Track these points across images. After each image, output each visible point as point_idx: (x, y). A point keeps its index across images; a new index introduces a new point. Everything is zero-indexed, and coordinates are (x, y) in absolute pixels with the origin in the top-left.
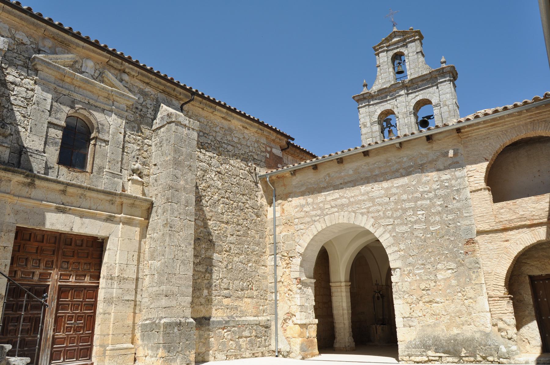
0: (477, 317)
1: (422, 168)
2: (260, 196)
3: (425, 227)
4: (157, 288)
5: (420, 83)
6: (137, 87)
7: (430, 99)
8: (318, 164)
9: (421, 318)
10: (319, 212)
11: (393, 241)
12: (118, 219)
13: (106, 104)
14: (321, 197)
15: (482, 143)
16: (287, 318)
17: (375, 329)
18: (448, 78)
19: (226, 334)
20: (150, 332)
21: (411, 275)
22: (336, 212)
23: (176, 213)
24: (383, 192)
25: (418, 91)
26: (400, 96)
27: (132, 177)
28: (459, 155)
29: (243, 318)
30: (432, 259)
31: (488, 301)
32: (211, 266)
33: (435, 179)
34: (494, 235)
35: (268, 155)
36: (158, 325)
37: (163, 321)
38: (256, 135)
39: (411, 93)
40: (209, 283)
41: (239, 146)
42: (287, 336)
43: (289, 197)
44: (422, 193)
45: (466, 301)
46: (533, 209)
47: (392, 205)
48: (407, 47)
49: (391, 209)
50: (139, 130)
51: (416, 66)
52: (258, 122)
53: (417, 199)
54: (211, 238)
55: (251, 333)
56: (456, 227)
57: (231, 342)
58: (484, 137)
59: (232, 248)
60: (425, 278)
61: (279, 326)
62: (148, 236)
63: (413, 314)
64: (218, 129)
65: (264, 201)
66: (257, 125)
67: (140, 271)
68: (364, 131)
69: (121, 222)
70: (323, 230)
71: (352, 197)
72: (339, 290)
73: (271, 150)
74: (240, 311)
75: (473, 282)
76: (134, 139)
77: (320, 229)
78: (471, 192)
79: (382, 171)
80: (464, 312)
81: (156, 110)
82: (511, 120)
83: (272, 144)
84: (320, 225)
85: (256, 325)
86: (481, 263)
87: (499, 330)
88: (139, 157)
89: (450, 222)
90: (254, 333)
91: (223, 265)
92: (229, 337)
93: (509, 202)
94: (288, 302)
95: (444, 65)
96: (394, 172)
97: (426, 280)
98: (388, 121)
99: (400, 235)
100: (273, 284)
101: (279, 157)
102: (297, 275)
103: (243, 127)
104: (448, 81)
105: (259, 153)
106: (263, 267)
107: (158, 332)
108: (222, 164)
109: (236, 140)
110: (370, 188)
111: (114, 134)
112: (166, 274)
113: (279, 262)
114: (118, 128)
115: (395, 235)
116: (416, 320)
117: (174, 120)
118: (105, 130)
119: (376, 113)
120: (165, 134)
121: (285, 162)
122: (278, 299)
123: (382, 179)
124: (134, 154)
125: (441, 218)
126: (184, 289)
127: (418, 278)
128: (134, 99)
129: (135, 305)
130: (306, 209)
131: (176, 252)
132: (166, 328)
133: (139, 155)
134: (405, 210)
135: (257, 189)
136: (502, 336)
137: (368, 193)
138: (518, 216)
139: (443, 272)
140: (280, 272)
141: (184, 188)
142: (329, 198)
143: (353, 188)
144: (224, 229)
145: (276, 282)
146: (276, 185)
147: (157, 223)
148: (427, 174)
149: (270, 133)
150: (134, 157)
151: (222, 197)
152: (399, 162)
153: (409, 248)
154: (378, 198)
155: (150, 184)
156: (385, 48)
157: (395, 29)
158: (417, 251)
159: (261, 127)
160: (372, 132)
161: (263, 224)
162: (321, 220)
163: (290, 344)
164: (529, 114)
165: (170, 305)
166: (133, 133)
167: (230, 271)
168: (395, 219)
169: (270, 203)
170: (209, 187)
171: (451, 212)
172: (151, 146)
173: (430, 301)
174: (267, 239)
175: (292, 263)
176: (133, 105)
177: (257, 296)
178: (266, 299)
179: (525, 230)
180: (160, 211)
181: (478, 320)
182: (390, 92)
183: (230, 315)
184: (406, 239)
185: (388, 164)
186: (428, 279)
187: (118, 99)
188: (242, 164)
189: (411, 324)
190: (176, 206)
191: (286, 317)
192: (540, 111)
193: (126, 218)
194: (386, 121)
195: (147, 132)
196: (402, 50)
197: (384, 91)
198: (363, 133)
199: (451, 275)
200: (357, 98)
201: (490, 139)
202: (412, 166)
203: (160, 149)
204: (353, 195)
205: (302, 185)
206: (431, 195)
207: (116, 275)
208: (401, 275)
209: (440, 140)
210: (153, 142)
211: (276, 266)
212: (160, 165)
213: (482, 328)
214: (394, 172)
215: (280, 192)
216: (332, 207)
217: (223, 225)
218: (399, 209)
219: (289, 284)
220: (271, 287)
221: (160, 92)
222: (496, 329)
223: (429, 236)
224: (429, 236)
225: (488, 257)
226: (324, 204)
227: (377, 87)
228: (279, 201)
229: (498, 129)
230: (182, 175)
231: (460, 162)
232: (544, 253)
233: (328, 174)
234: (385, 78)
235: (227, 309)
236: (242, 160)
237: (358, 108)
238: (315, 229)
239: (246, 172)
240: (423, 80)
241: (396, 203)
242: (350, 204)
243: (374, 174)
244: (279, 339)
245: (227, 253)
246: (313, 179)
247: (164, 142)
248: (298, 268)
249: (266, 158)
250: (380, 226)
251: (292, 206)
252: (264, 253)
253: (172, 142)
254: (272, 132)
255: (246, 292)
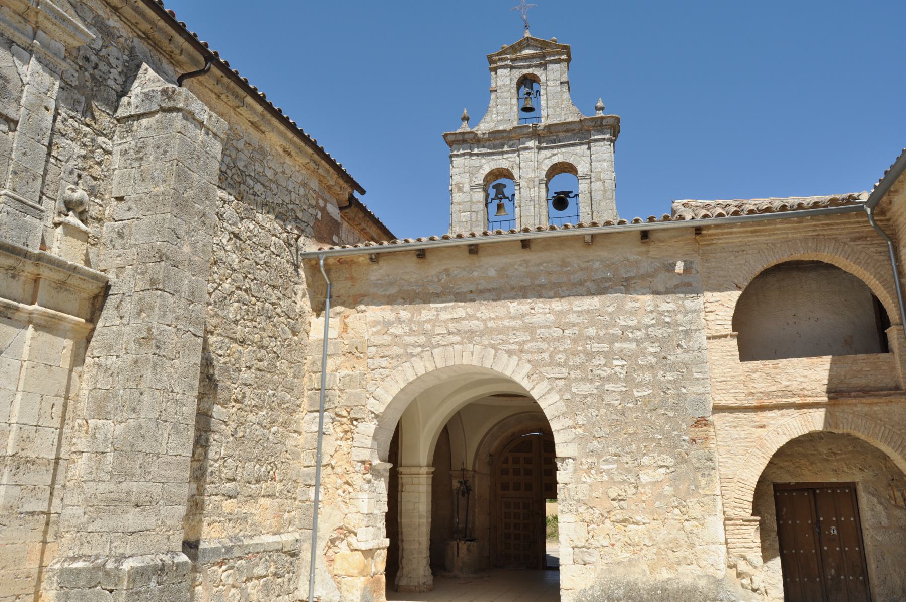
0: (704, 552)
1: (627, 285)
2: (300, 294)
3: (624, 389)
4: (112, 486)
5: (561, 135)
6: (91, 9)
7: (575, 164)
8: (428, 249)
9: (606, 549)
10: (422, 339)
11: (564, 409)
12: (23, 316)
13: (16, 29)
14: (428, 312)
15: (732, 258)
16: (337, 538)
17: (455, 548)
18: (607, 136)
19: (226, 573)
20: (86, 591)
21: (593, 472)
22: (457, 343)
23: (170, 317)
24: (552, 317)
25: (557, 147)
26: (526, 149)
27: (63, 219)
28: (694, 272)
29: (256, 540)
30: (634, 447)
31: (725, 525)
32: (206, 432)
33: (649, 308)
34: (741, 415)
35: (319, 216)
36: (113, 576)
37: (127, 566)
38: (304, 172)
39: (545, 148)
40: (200, 468)
41: (274, 186)
42: (336, 572)
43: (361, 303)
44: (624, 329)
45: (686, 524)
46: (803, 379)
47: (568, 344)
48: (546, 69)
49: (565, 351)
50: (88, 111)
51: (556, 105)
52: (313, 145)
53: (613, 339)
54: (211, 371)
55: (267, 568)
56: (678, 395)
57: (233, 591)
58: (736, 249)
59: (247, 394)
60: (618, 478)
61: (319, 552)
62: (88, 360)
63: (591, 541)
64: (240, 145)
65: (304, 304)
66: (309, 150)
67: (64, 441)
68: (457, 197)
69: (30, 322)
70: (427, 374)
71: (491, 319)
72: (415, 480)
73: (325, 206)
74: (251, 525)
75: (700, 491)
76: (75, 130)
77: (421, 372)
78: (708, 338)
79: (554, 279)
80: (682, 542)
81: (130, 74)
82: (785, 228)
83: (327, 196)
84: (422, 364)
85: (277, 551)
86: (716, 460)
87: (739, 575)
88: (84, 174)
89: (669, 386)
90: (272, 569)
91: (228, 431)
92: (230, 581)
93: (766, 362)
94: (343, 506)
95: (601, 114)
96: (574, 285)
97: (620, 483)
98: (499, 188)
99: (578, 399)
100: (312, 470)
101: (336, 221)
102: (366, 455)
103: (284, 151)
104: (608, 140)
105: (305, 207)
106: (295, 435)
107: (111, 591)
108: (242, 219)
109: (269, 173)
110: (528, 307)
111: (30, 109)
112: (141, 455)
113: (328, 426)
114: (43, 95)
115: (569, 397)
116: (596, 553)
117: (181, 105)
118: (10, 93)
119: (481, 171)
120: (152, 133)
121: (347, 236)
122: (320, 498)
123: (552, 294)
124: (71, 164)
125: (655, 376)
126: (172, 487)
127: (606, 478)
128: (87, 35)
129: (47, 524)
130: (396, 330)
131: (164, 405)
132: (134, 581)
133: (84, 169)
134: (590, 356)
135: (296, 279)
136: (742, 585)
137: (523, 316)
138: (779, 386)
139: (650, 472)
140: (328, 446)
141: (190, 261)
142: (444, 316)
143: (494, 303)
144: (236, 355)
145: (318, 464)
146: (333, 275)
147: (120, 334)
148: (635, 296)
149: (329, 172)
150: (71, 172)
151: (238, 288)
152: (586, 269)
153: (594, 424)
154: (541, 327)
155: (103, 241)
156: (509, 63)
157: (527, 34)
158: (607, 430)
159: (316, 156)
160: (471, 202)
161: (300, 348)
162: (426, 355)
163: (339, 589)
164: (814, 223)
165: (143, 527)
166: (74, 114)
167: (240, 441)
168: (572, 368)
169: (319, 309)
170: (216, 263)
171: (673, 367)
172: (110, 153)
173: (624, 521)
174: (305, 379)
175: (356, 430)
176: (79, 49)
177: (281, 492)
178: (295, 499)
179: (792, 411)
180: (128, 306)
181: (705, 556)
182: (510, 139)
183: (232, 534)
184: (589, 407)
185: (565, 269)
186: (624, 481)
187: (49, 25)
188: (276, 225)
189: (587, 558)
190: (171, 300)
191: (335, 536)
192: (832, 222)
193: (44, 314)
194: (498, 187)
195: (105, 121)
196: (538, 72)
197: (500, 136)
198: (455, 201)
199: (663, 477)
200: (450, 138)
201: (747, 254)
202: (609, 279)
203: (137, 164)
204: (493, 315)
205: (391, 284)
206: (639, 334)
207: (10, 452)
208: (575, 471)
209: (663, 242)
210: (116, 145)
211: (321, 433)
212: (136, 202)
213: (711, 571)
214: (574, 285)
215: (342, 291)
216: (450, 333)
217: (235, 346)
218: (580, 352)
219: (347, 472)
220: (308, 475)
221: (139, 36)
222: (733, 572)
223: (630, 405)
224: (630, 405)
225: (729, 452)
226: (434, 326)
227: (486, 125)
228: (339, 309)
229: (762, 239)
230: (187, 233)
231: (694, 284)
232: (801, 449)
233: (447, 270)
234: (504, 114)
235: (230, 521)
236: (277, 217)
237: (451, 156)
238: (411, 370)
239: (282, 242)
240: (567, 131)
241: (575, 341)
242: (487, 331)
243: (537, 282)
244: (318, 579)
245: (238, 405)
246: (415, 276)
247: (149, 150)
248: (369, 442)
249: (316, 219)
250: (542, 380)
251: (367, 320)
252: (299, 406)
253: (173, 152)
254: (332, 170)
255: (264, 486)
